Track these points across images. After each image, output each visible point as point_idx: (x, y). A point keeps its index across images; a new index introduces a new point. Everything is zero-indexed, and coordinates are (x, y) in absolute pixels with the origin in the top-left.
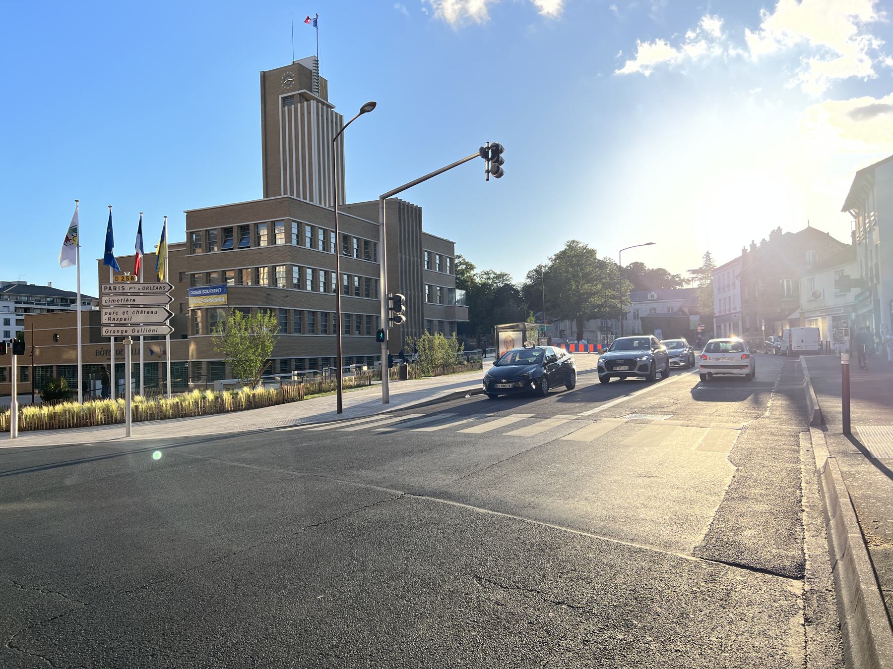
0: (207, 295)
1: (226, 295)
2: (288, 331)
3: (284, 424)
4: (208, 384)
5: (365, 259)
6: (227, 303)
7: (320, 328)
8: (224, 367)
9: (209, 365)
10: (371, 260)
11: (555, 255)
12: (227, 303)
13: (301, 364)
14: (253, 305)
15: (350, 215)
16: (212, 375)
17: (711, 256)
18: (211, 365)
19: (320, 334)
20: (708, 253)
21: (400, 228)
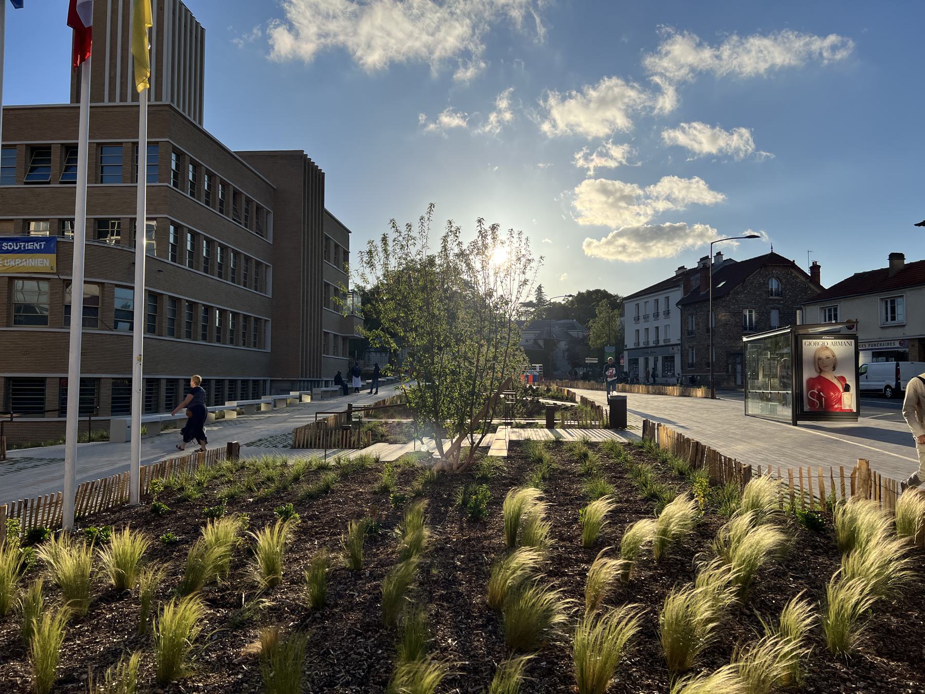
0: (13, 251)
1: (55, 255)
2: (192, 336)
3: (638, 407)
4: (92, 418)
5: (234, 219)
6: (55, 271)
7: (166, 325)
8: (43, 390)
9: (9, 385)
10: (240, 223)
11: (428, 256)
12: (55, 271)
13: (172, 389)
14: (106, 279)
15: (244, 162)
16: (13, 404)
17: (543, 290)
18: (13, 385)
19: (165, 336)
20: (540, 286)
21: (304, 194)
